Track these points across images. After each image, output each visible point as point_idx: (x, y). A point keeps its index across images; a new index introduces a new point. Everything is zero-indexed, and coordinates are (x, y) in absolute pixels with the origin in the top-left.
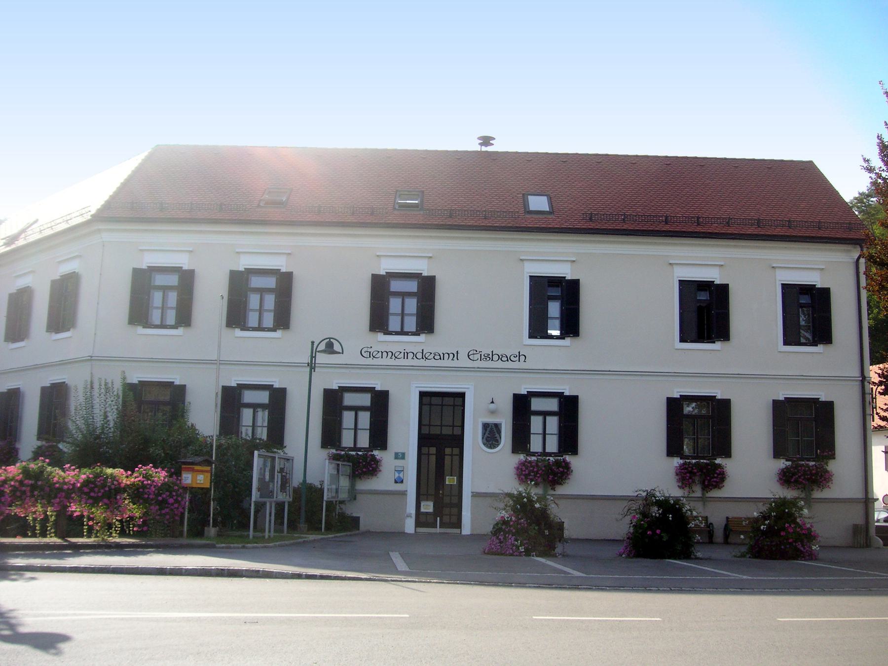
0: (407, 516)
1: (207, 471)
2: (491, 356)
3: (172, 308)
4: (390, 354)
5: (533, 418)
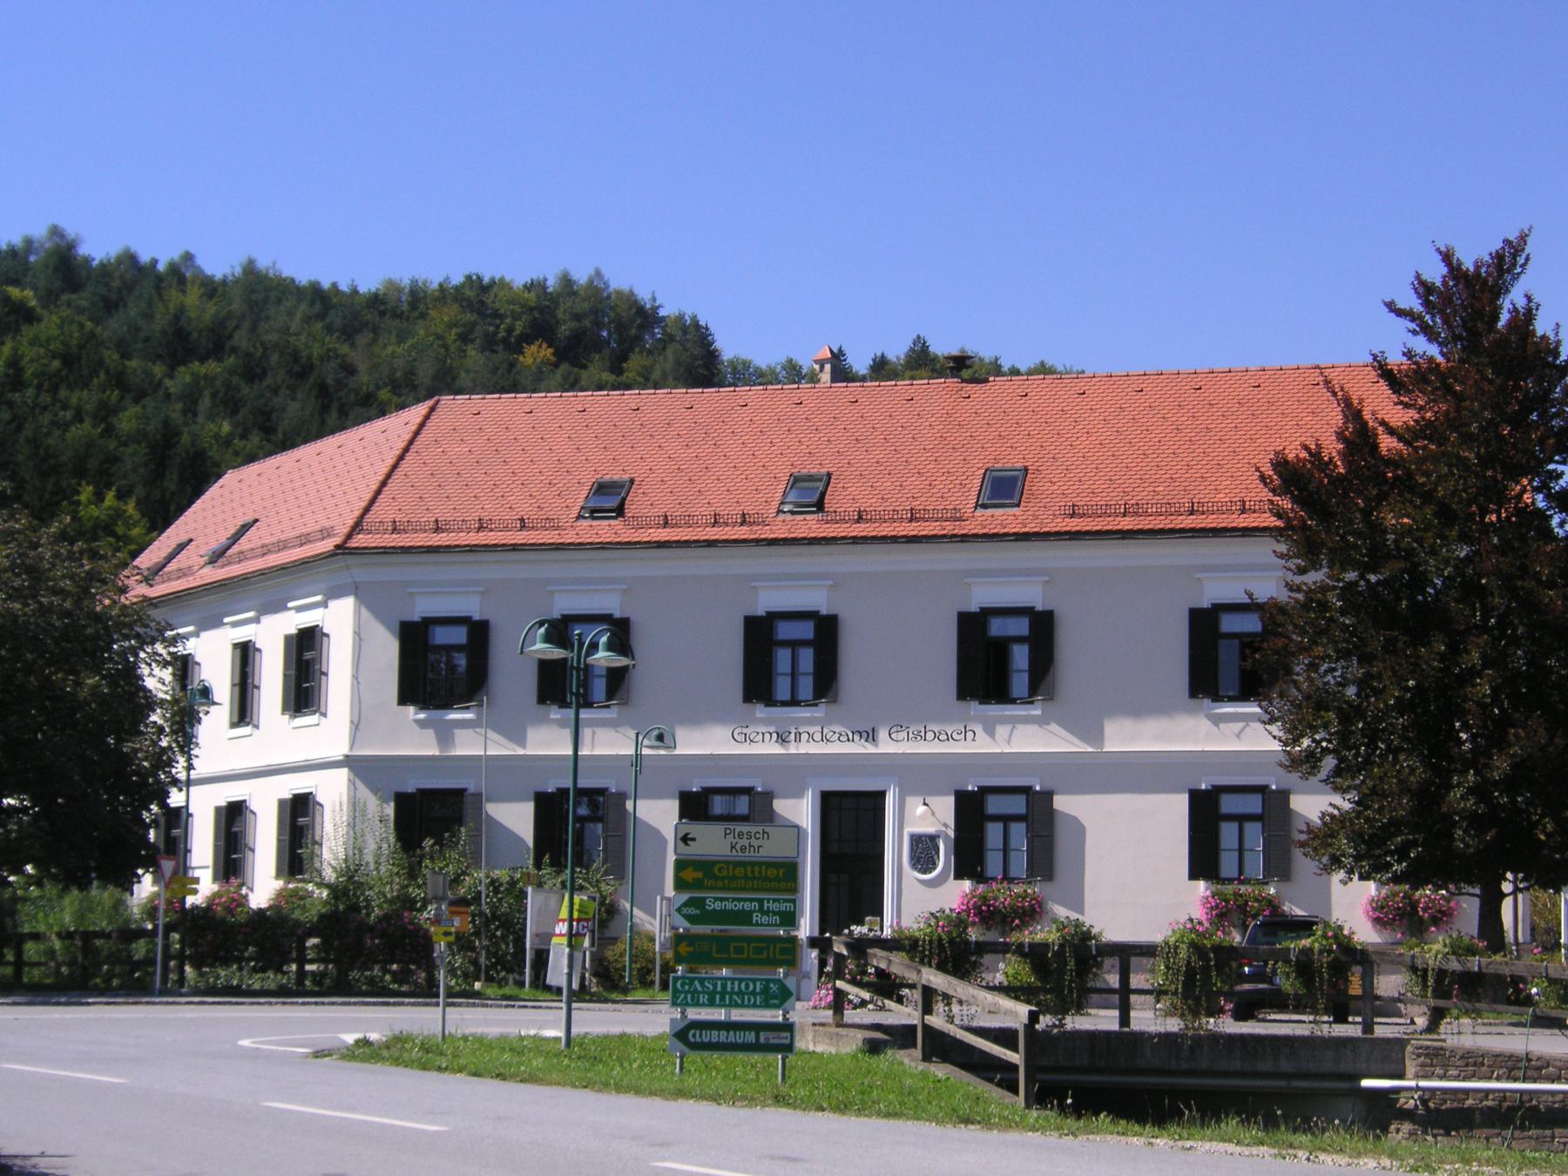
0: (804, 977)
2: (923, 734)
3: (601, 676)
4: (775, 735)
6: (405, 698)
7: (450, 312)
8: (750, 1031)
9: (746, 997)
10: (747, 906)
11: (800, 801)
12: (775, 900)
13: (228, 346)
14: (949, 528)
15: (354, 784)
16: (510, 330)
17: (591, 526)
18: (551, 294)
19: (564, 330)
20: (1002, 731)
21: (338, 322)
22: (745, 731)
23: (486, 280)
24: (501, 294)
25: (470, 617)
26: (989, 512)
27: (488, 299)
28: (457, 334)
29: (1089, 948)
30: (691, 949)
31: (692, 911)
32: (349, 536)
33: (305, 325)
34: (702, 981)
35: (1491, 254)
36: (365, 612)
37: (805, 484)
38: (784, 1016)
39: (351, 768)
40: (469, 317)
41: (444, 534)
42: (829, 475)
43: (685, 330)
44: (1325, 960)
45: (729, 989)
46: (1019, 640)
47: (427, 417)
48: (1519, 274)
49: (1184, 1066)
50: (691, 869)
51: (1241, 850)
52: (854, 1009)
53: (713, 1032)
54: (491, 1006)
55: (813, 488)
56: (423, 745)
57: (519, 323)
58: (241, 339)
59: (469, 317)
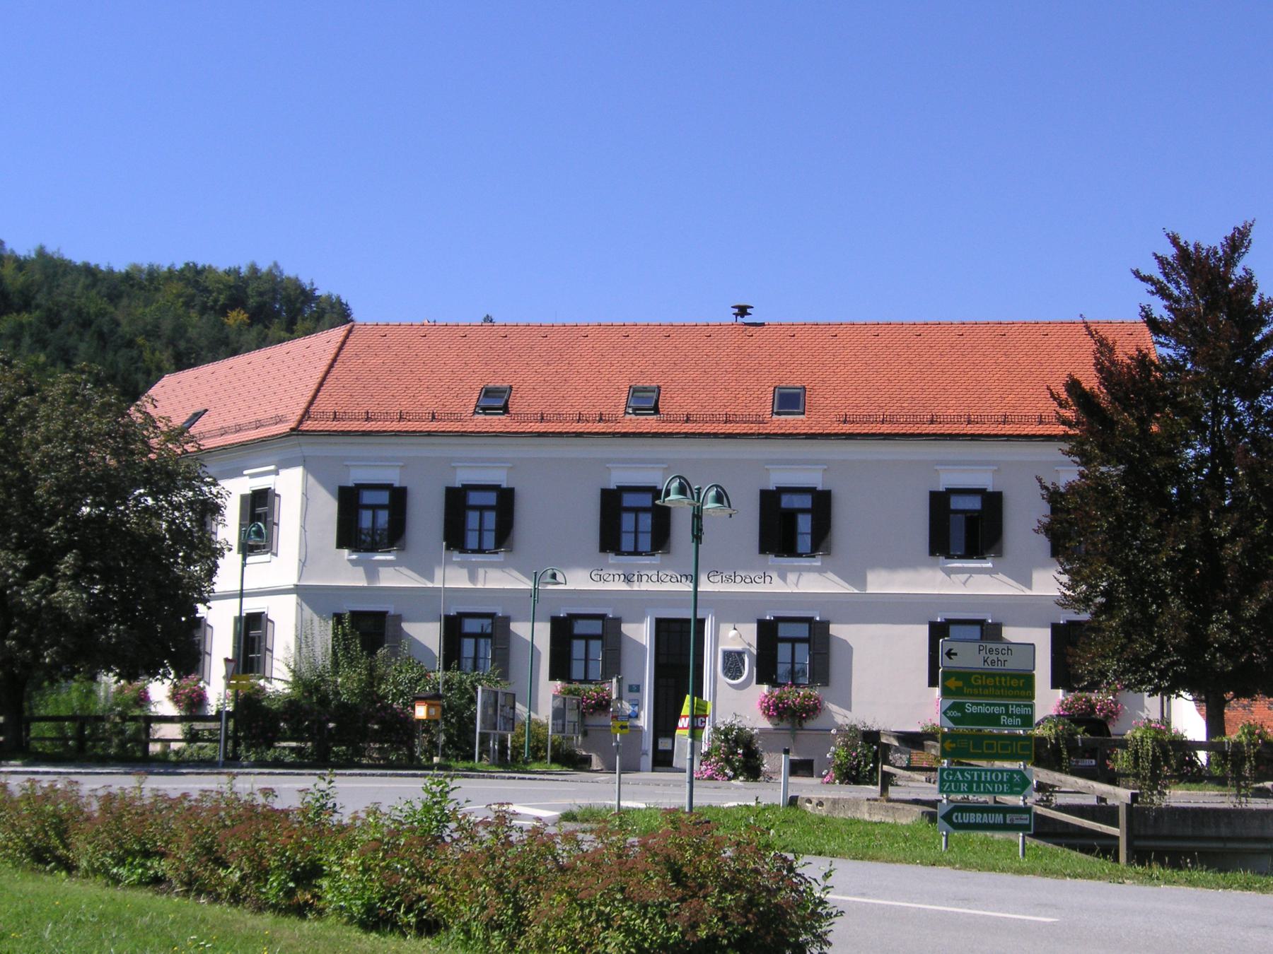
0: (643, 754)
1: (438, 705)
2: (733, 578)
4: (622, 577)
5: (780, 645)
6: (341, 544)
7: (176, 287)
8: (999, 813)
9: (996, 785)
10: (996, 710)
11: (641, 625)
12: (1018, 706)
13: (33, 303)
14: (755, 428)
15: (301, 606)
16: (216, 301)
17: (499, 420)
18: (243, 277)
19: (252, 302)
20: (792, 577)
21: (104, 290)
22: (600, 573)
23: (200, 266)
24: (210, 276)
25: (392, 484)
26: (783, 417)
27: (201, 279)
28: (182, 302)
29: (1076, 741)
30: (954, 745)
31: (955, 714)
32: (300, 422)
33: (85, 292)
34: (962, 772)
35: (1226, 238)
36: (311, 479)
37: (641, 394)
38: (1024, 800)
39: (297, 594)
40: (190, 291)
41: (373, 423)
42: (659, 388)
43: (332, 305)
44: (1252, 751)
45: (983, 779)
46: (804, 511)
47: (347, 337)
48: (1244, 253)
49: (1150, 832)
50: (954, 679)
51: (586, 659)
52: (728, 780)
53: (971, 814)
54: (497, 778)
55: (648, 397)
56: (356, 579)
57: (222, 296)
58: (41, 298)
59: (190, 291)
